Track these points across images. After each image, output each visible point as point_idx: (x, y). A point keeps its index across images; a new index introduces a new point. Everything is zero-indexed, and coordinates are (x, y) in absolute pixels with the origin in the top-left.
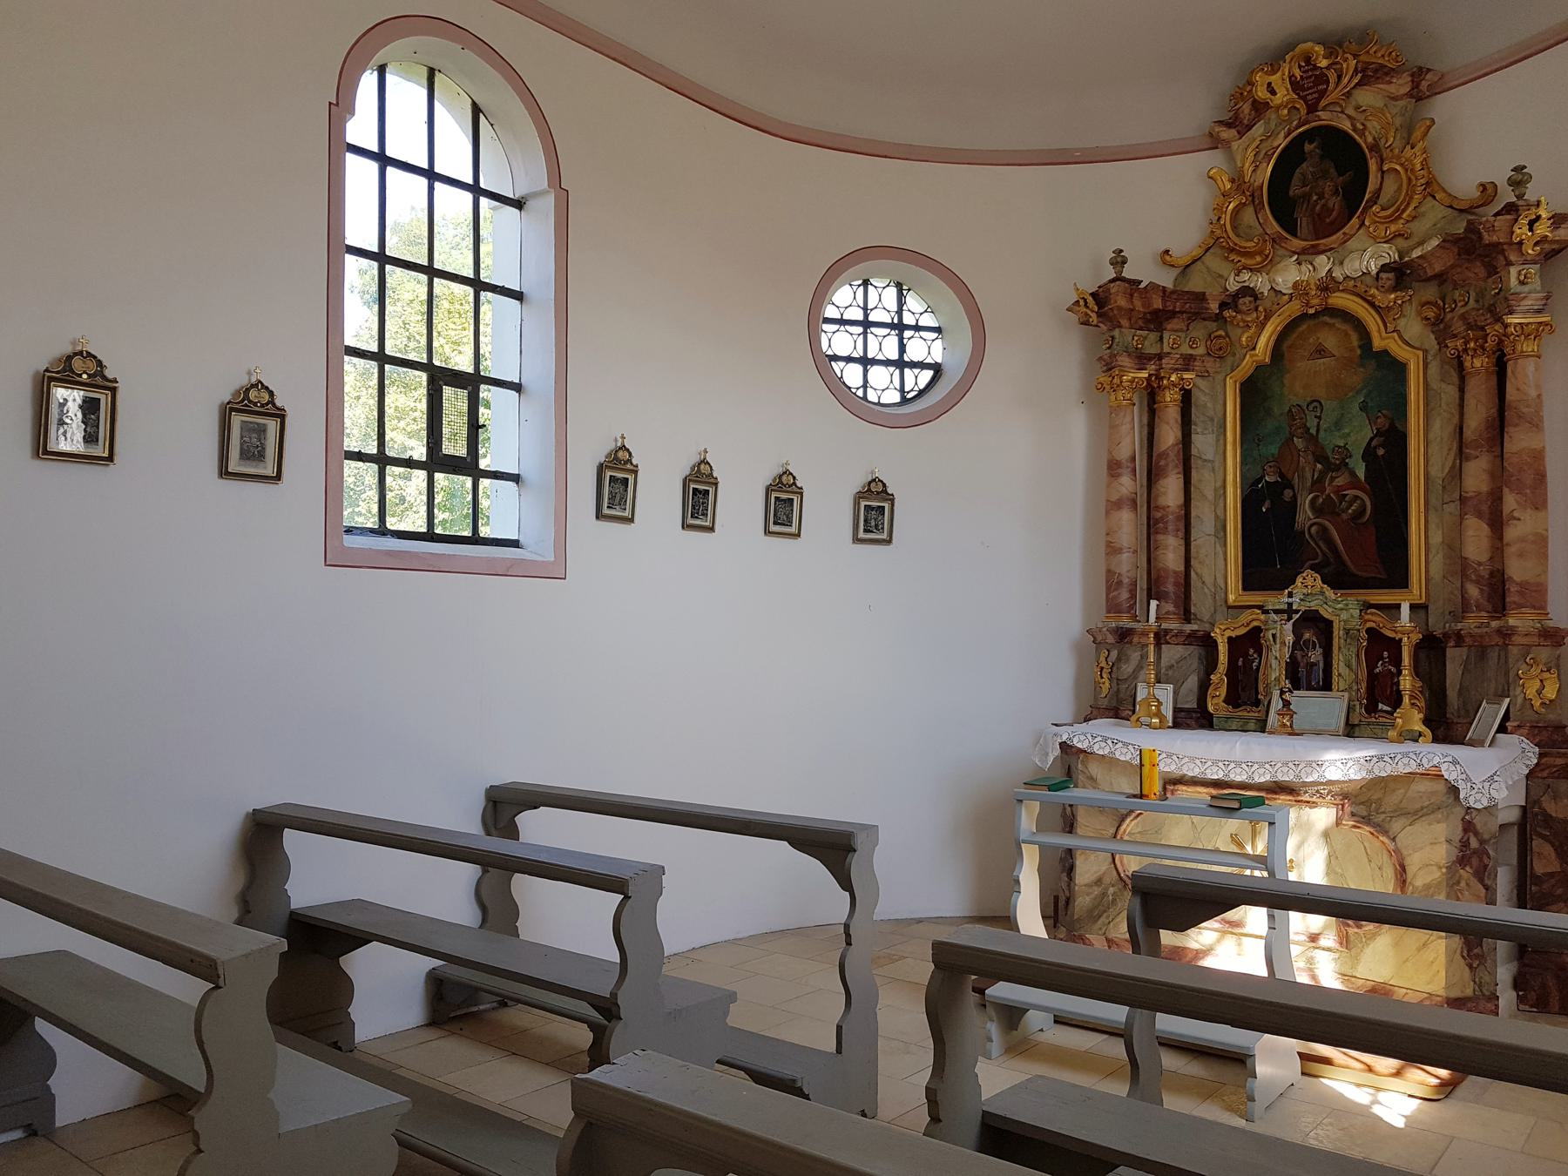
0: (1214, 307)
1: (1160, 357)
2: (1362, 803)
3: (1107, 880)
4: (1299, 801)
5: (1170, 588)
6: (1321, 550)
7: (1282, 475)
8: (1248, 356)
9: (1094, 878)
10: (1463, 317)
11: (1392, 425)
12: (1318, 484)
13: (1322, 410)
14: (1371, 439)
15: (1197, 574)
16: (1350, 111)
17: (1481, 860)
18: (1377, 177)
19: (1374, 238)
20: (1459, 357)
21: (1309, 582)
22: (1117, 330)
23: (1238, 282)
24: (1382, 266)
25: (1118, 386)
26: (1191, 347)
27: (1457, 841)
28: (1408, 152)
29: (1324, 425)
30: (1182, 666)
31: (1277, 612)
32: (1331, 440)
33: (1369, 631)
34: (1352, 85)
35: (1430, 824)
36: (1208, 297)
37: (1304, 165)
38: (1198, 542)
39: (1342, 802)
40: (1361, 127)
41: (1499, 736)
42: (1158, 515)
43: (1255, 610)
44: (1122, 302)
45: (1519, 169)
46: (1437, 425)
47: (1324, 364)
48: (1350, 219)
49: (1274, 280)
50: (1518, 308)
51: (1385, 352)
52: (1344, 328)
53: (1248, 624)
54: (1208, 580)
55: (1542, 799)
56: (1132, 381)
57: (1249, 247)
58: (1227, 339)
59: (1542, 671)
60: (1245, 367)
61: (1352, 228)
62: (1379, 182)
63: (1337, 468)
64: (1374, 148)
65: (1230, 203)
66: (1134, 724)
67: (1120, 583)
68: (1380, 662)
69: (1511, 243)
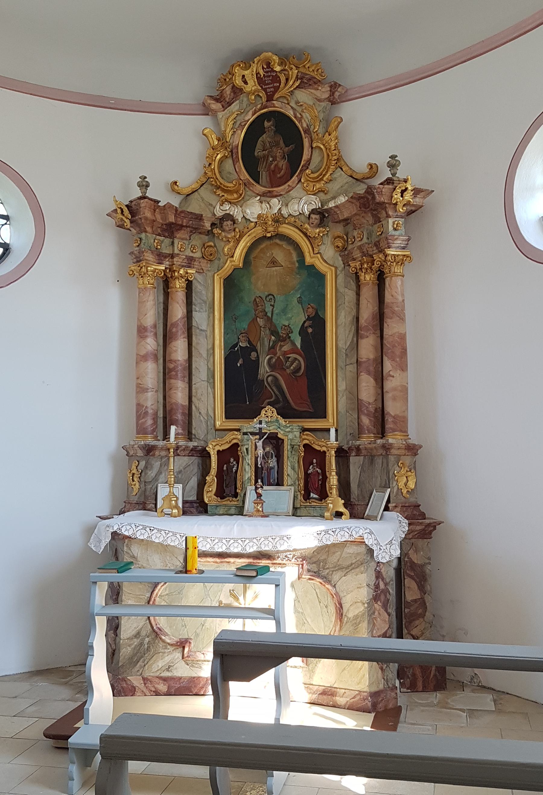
0: (208, 225)
1: (172, 256)
2: (314, 563)
3: (143, 633)
4: (274, 564)
5: (179, 417)
6: (274, 393)
7: (249, 342)
8: (228, 261)
9: (134, 633)
10: (360, 248)
11: (317, 313)
12: (272, 349)
13: (275, 301)
14: (305, 322)
15: (196, 407)
16: (293, 104)
17: (386, 596)
18: (309, 151)
19: (307, 191)
20: (356, 273)
21: (269, 414)
22: (144, 234)
23: (222, 210)
24: (312, 210)
25: (144, 274)
26: (192, 252)
27: (373, 585)
28: (327, 137)
29: (276, 311)
30: (187, 471)
31: (253, 434)
32: (281, 322)
33: (305, 446)
34: (295, 86)
35: (357, 575)
36: (204, 218)
37: (264, 136)
38: (198, 385)
39: (302, 563)
40: (300, 116)
41: (385, 512)
42: (172, 366)
43: (235, 432)
44: (148, 214)
45: (393, 157)
46: (342, 314)
47: (276, 271)
48: (291, 178)
49: (245, 212)
50: (393, 245)
51: (312, 266)
52: (288, 248)
53: (230, 442)
54: (203, 412)
55: (409, 552)
56: (154, 271)
57: (230, 187)
58: (215, 249)
59: (407, 471)
60: (226, 269)
61: (293, 182)
62: (310, 155)
63: (284, 340)
64: (307, 131)
65: (218, 154)
66: (159, 514)
67: (146, 413)
68: (311, 466)
69: (390, 204)
